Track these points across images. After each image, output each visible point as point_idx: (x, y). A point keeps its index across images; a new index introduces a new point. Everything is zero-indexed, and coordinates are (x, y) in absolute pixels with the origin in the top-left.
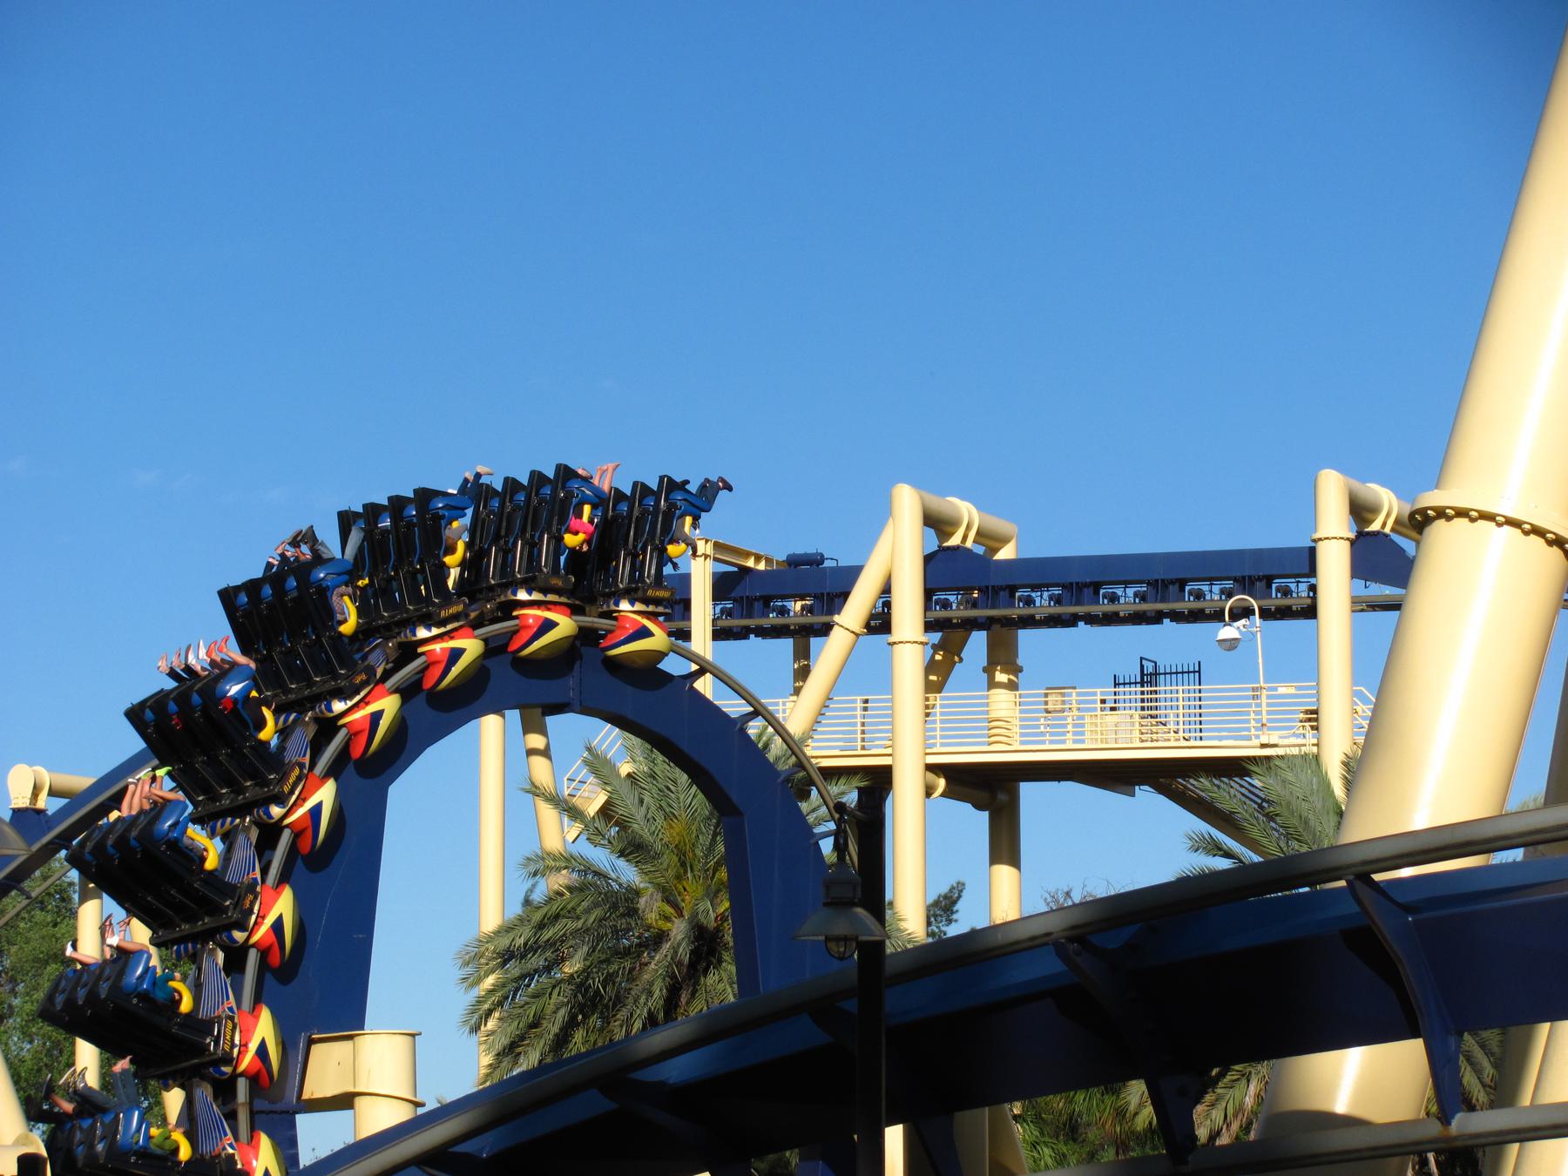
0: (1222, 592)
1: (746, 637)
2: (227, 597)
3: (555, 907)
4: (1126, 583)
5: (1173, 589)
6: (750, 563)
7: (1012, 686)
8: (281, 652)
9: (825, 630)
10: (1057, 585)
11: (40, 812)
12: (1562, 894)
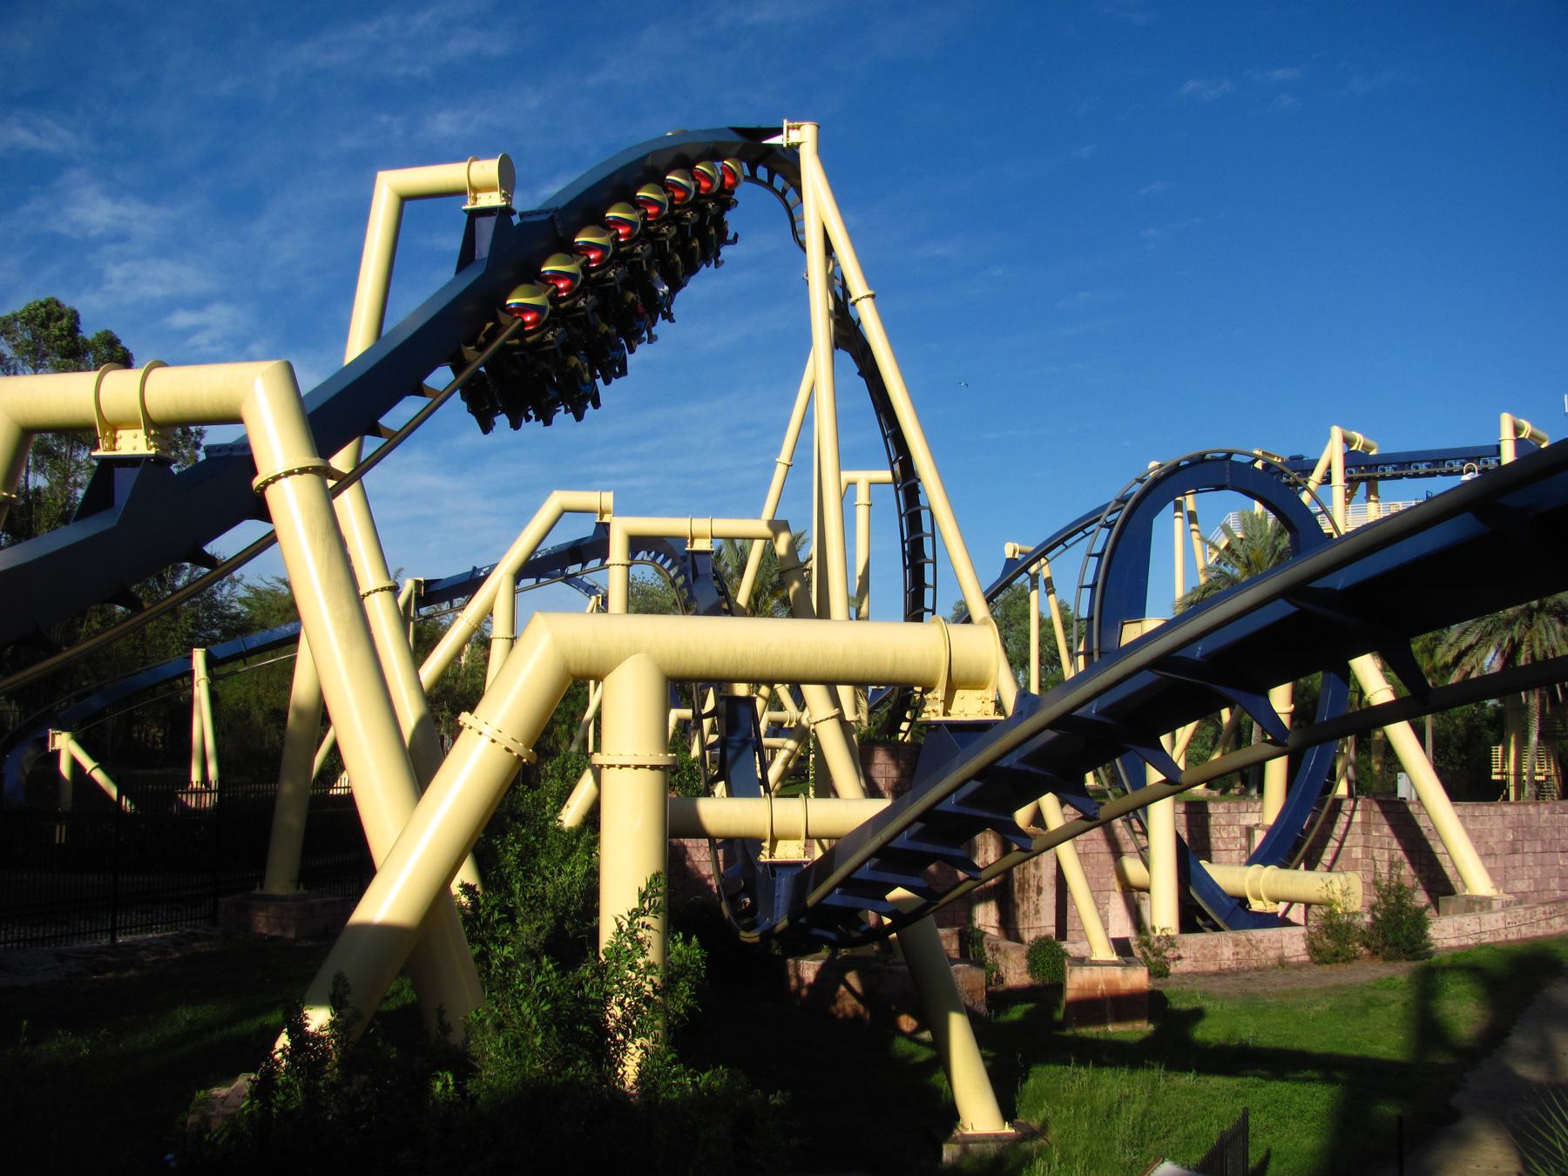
0: (1461, 463)
1: (1435, 476)
3: (1209, 585)
5: (1441, 463)
7: (1376, 502)
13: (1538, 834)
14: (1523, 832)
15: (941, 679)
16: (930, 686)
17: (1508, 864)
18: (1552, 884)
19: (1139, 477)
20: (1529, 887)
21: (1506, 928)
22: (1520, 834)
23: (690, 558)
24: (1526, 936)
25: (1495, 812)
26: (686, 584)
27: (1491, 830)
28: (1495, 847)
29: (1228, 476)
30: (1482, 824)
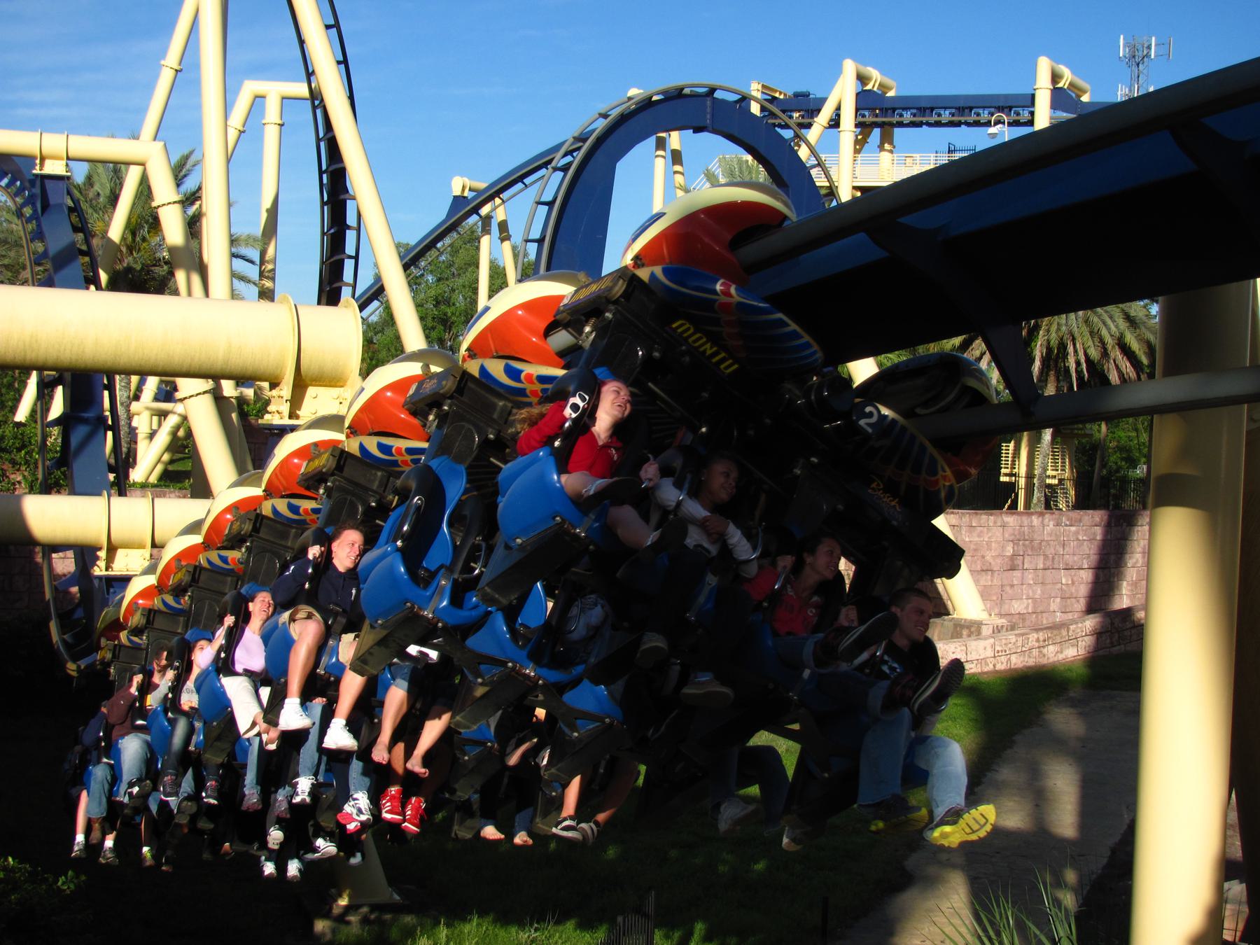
0: (989, 113)
1: (960, 126)
4: (945, 108)
6: (777, 95)
7: (891, 152)
9: (809, 126)
10: (914, 108)
11: (465, 197)
12: (64, 654)
13: (1040, 549)
14: (1024, 545)
15: (289, 369)
16: (276, 381)
17: (1005, 582)
18: (1052, 604)
19: (603, 111)
20: (1027, 607)
21: (995, 657)
22: (1021, 548)
23: (38, 183)
24: (1016, 666)
25: (995, 522)
26: (35, 216)
27: (989, 543)
28: (993, 563)
29: (708, 116)
30: (979, 536)
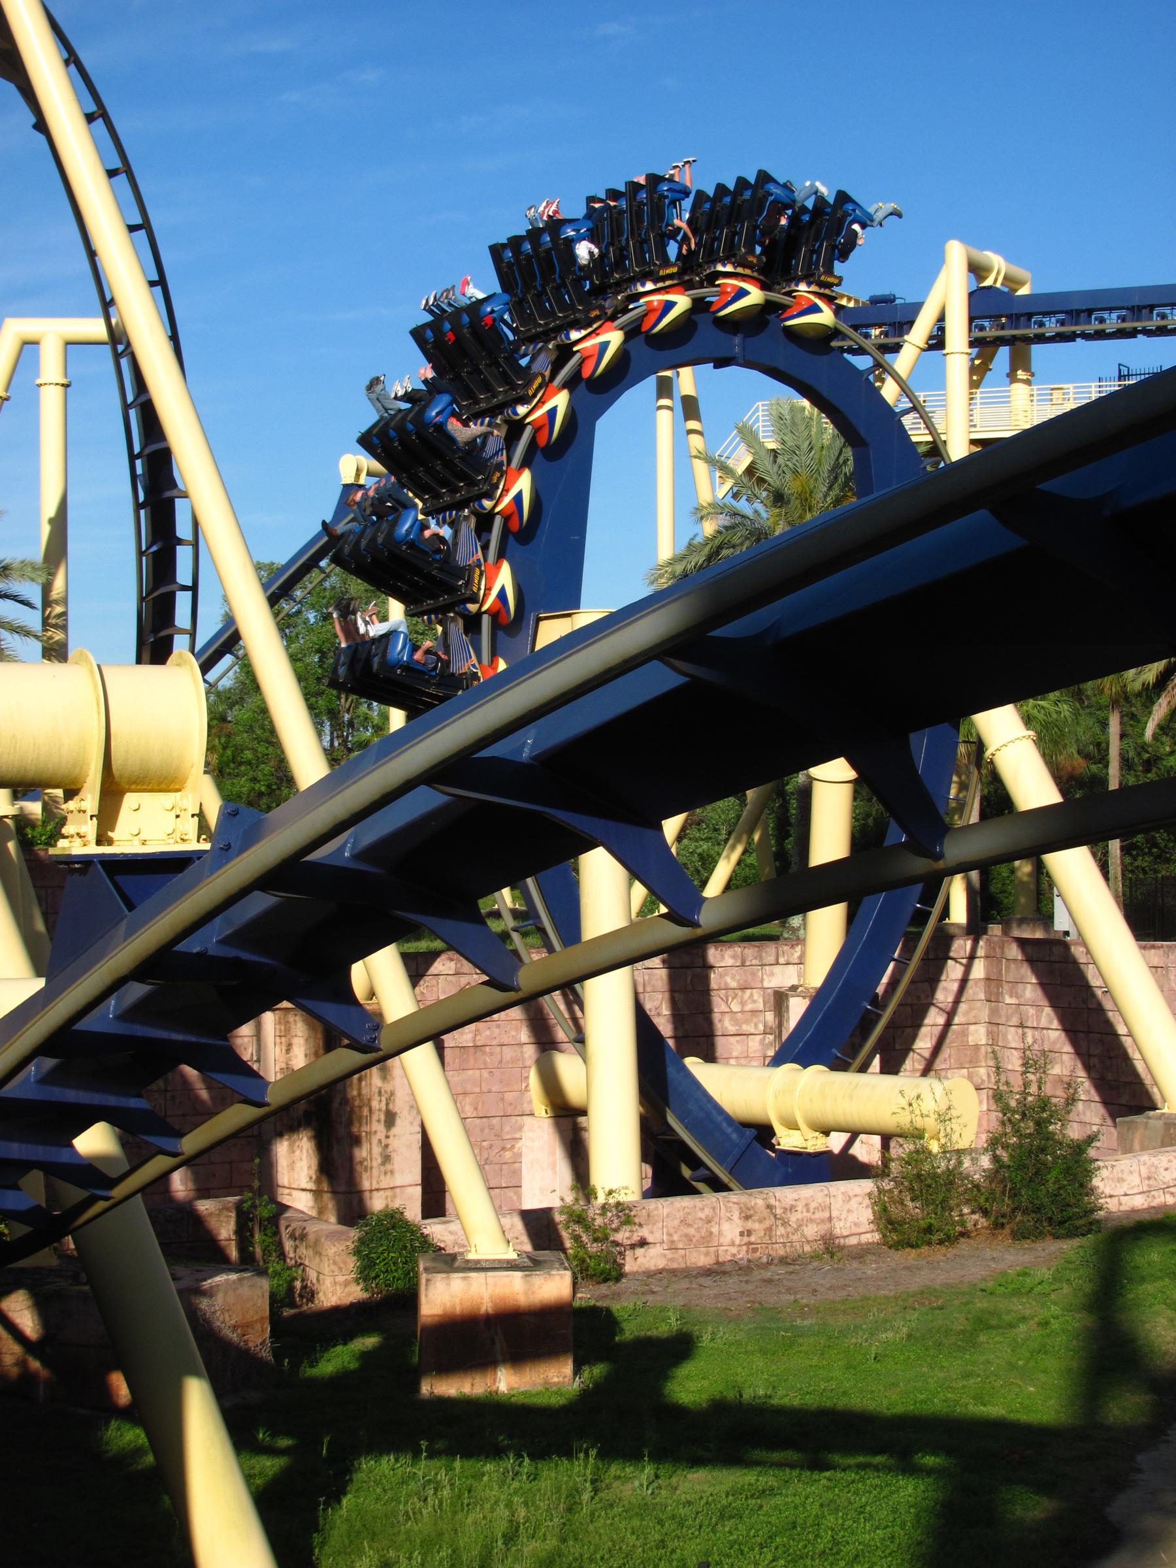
2: (496, 251)
4: (1111, 309)
7: (1027, 382)
8: (534, 294)
9: (896, 348)
